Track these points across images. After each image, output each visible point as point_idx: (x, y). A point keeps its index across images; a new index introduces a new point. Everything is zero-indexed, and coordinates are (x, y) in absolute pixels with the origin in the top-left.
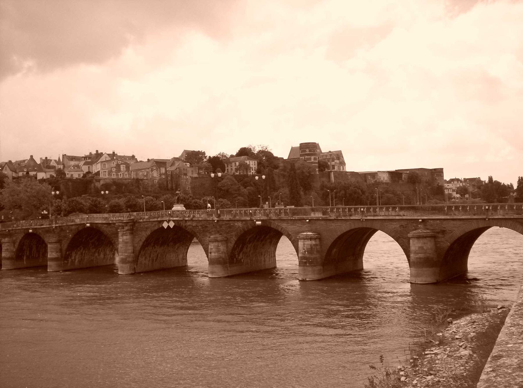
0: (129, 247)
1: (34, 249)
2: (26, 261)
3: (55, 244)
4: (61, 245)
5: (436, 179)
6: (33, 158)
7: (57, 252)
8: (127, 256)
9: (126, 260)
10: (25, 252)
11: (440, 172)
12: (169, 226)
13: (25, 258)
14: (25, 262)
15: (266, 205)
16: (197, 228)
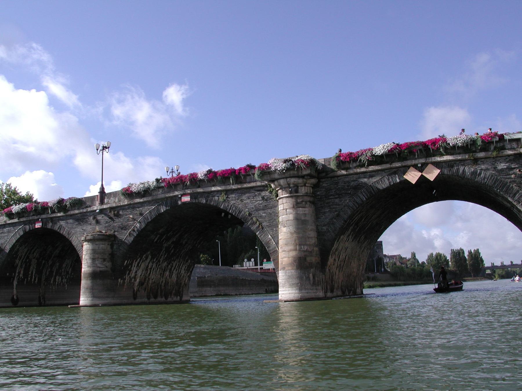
0: (310, 233)
1: (33, 269)
2: (16, 289)
3: (101, 242)
4: (112, 246)
5: (376, 251)
6: (14, 177)
7: (104, 260)
8: (307, 251)
9: (305, 259)
10: (17, 271)
11: (380, 245)
12: (422, 179)
13: (15, 283)
14: (15, 291)
15: (252, 262)
16: (511, 172)
